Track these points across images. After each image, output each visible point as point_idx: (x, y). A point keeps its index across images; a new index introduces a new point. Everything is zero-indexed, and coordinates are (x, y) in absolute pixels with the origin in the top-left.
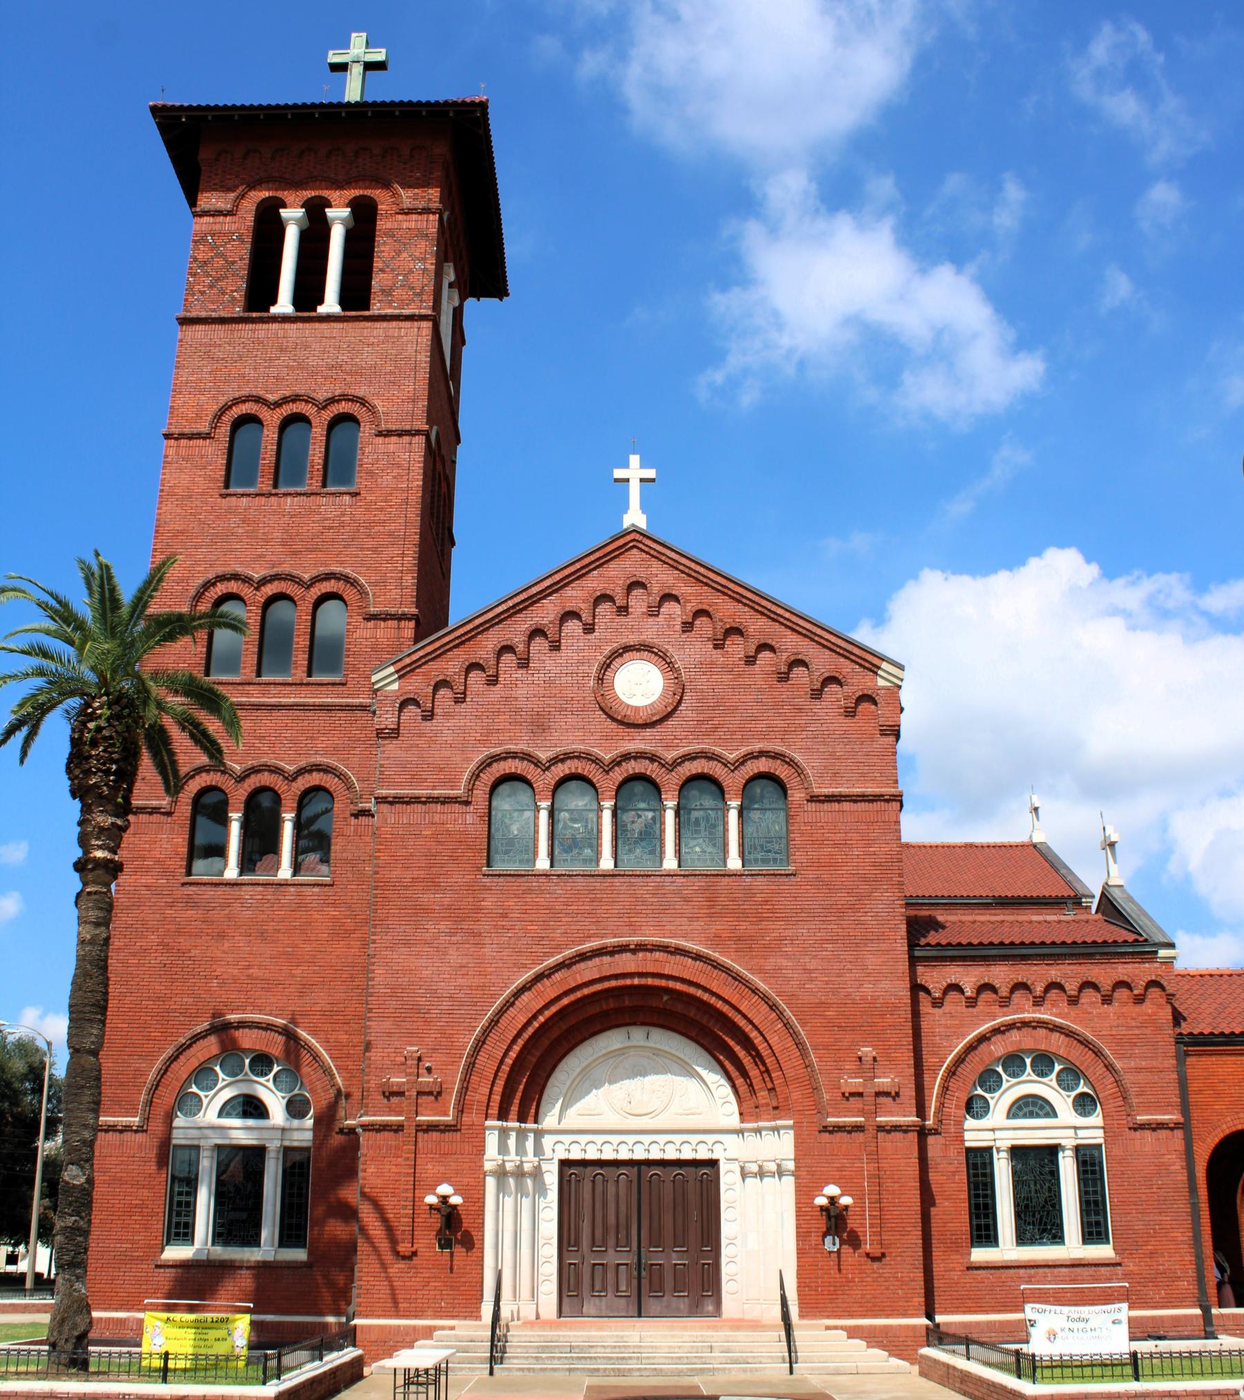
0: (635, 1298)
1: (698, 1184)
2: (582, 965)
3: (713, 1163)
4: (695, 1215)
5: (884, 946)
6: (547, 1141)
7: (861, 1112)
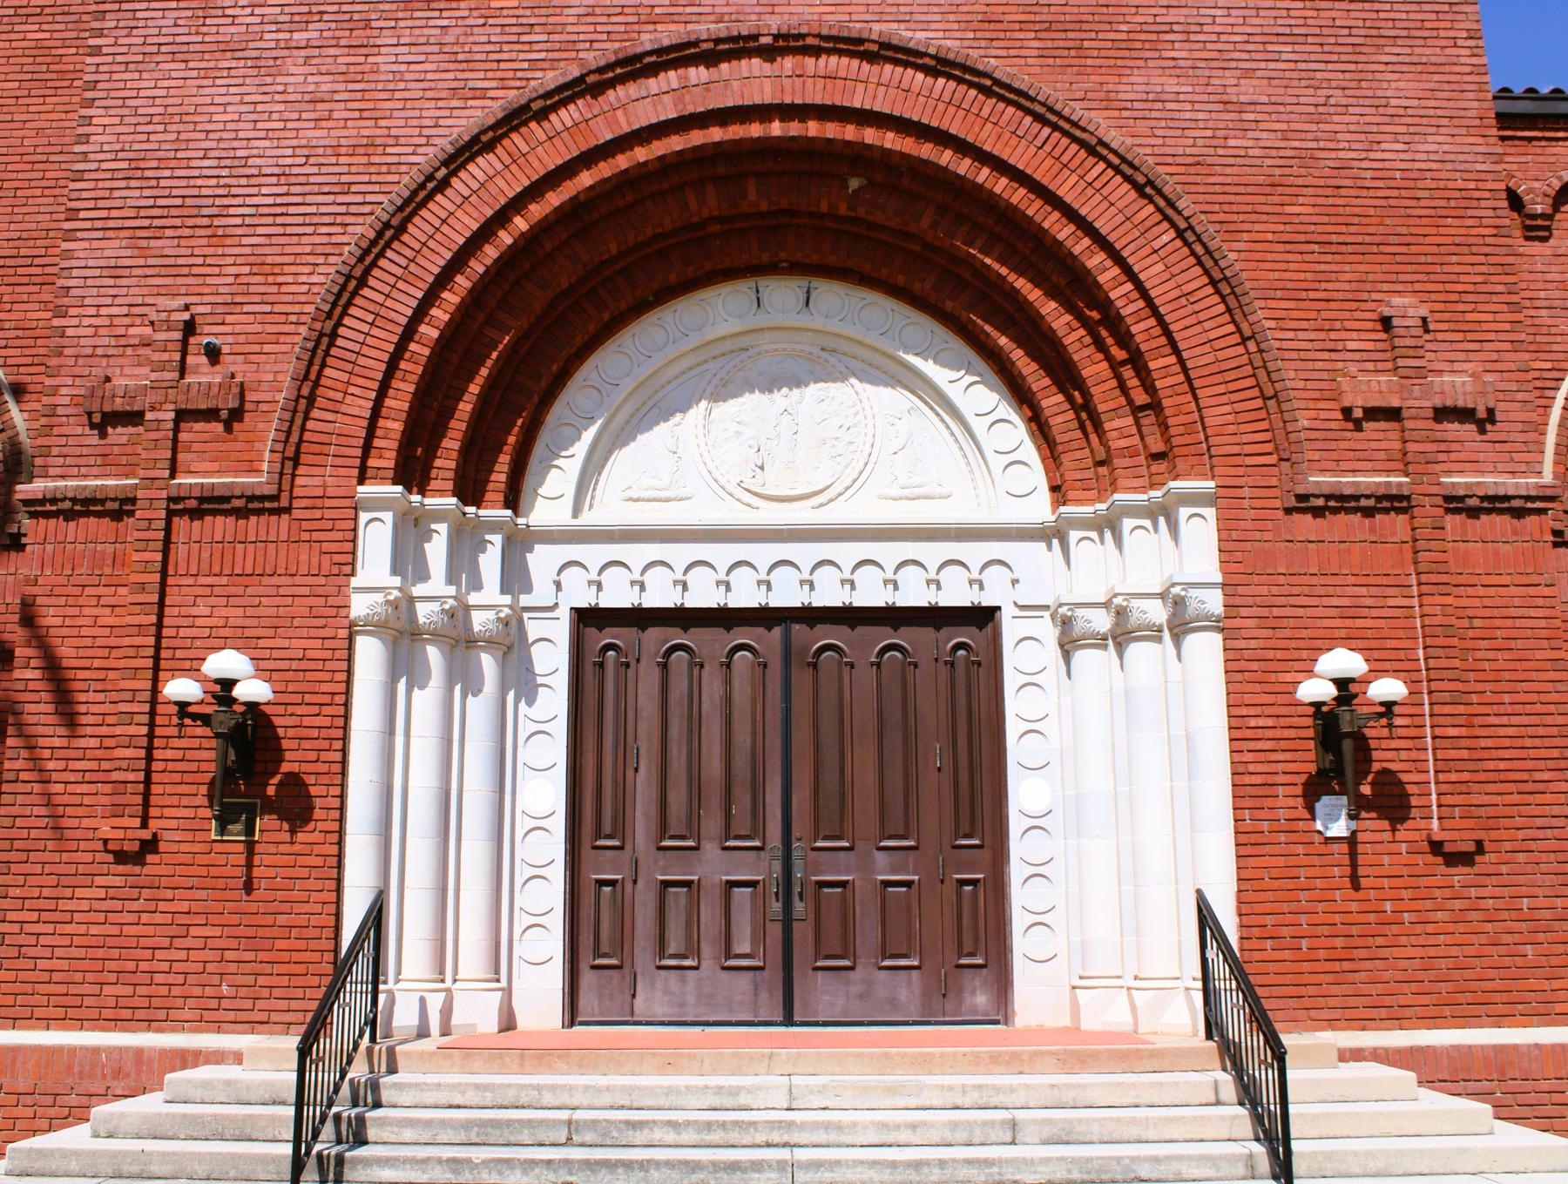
0: (774, 974)
1: (944, 672)
2: (632, 90)
3: (984, 617)
4: (935, 753)
5: (1428, 54)
6: (542, 561)
7: (1404, 462)
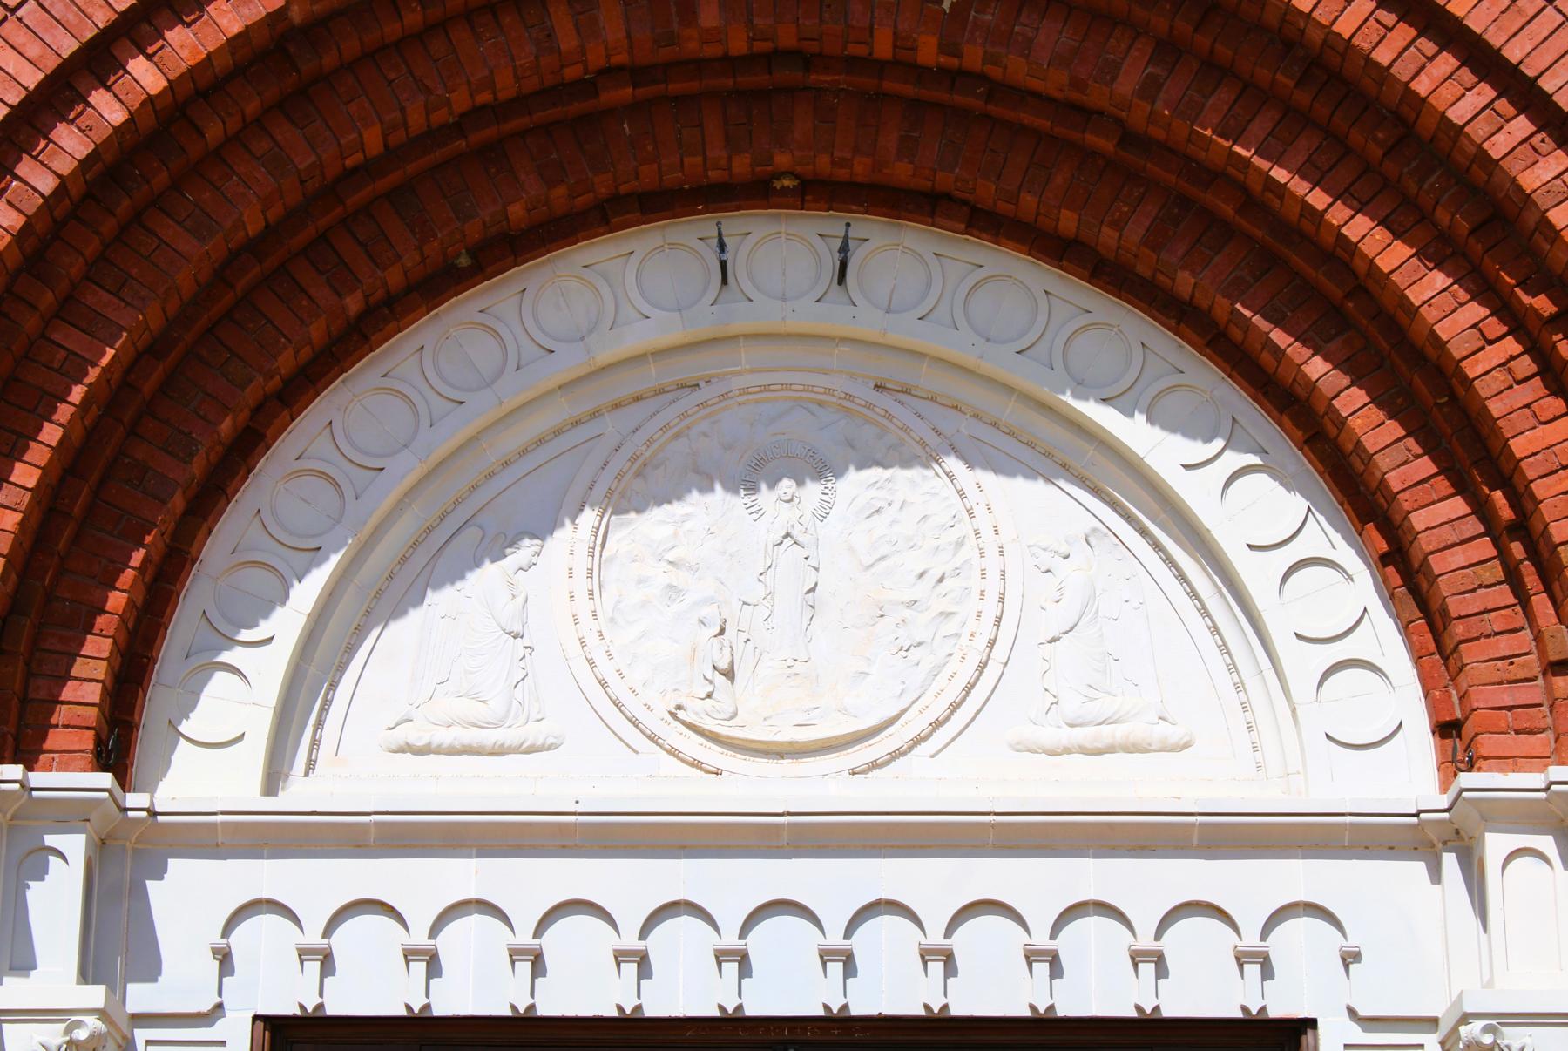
6: (187, 899)
